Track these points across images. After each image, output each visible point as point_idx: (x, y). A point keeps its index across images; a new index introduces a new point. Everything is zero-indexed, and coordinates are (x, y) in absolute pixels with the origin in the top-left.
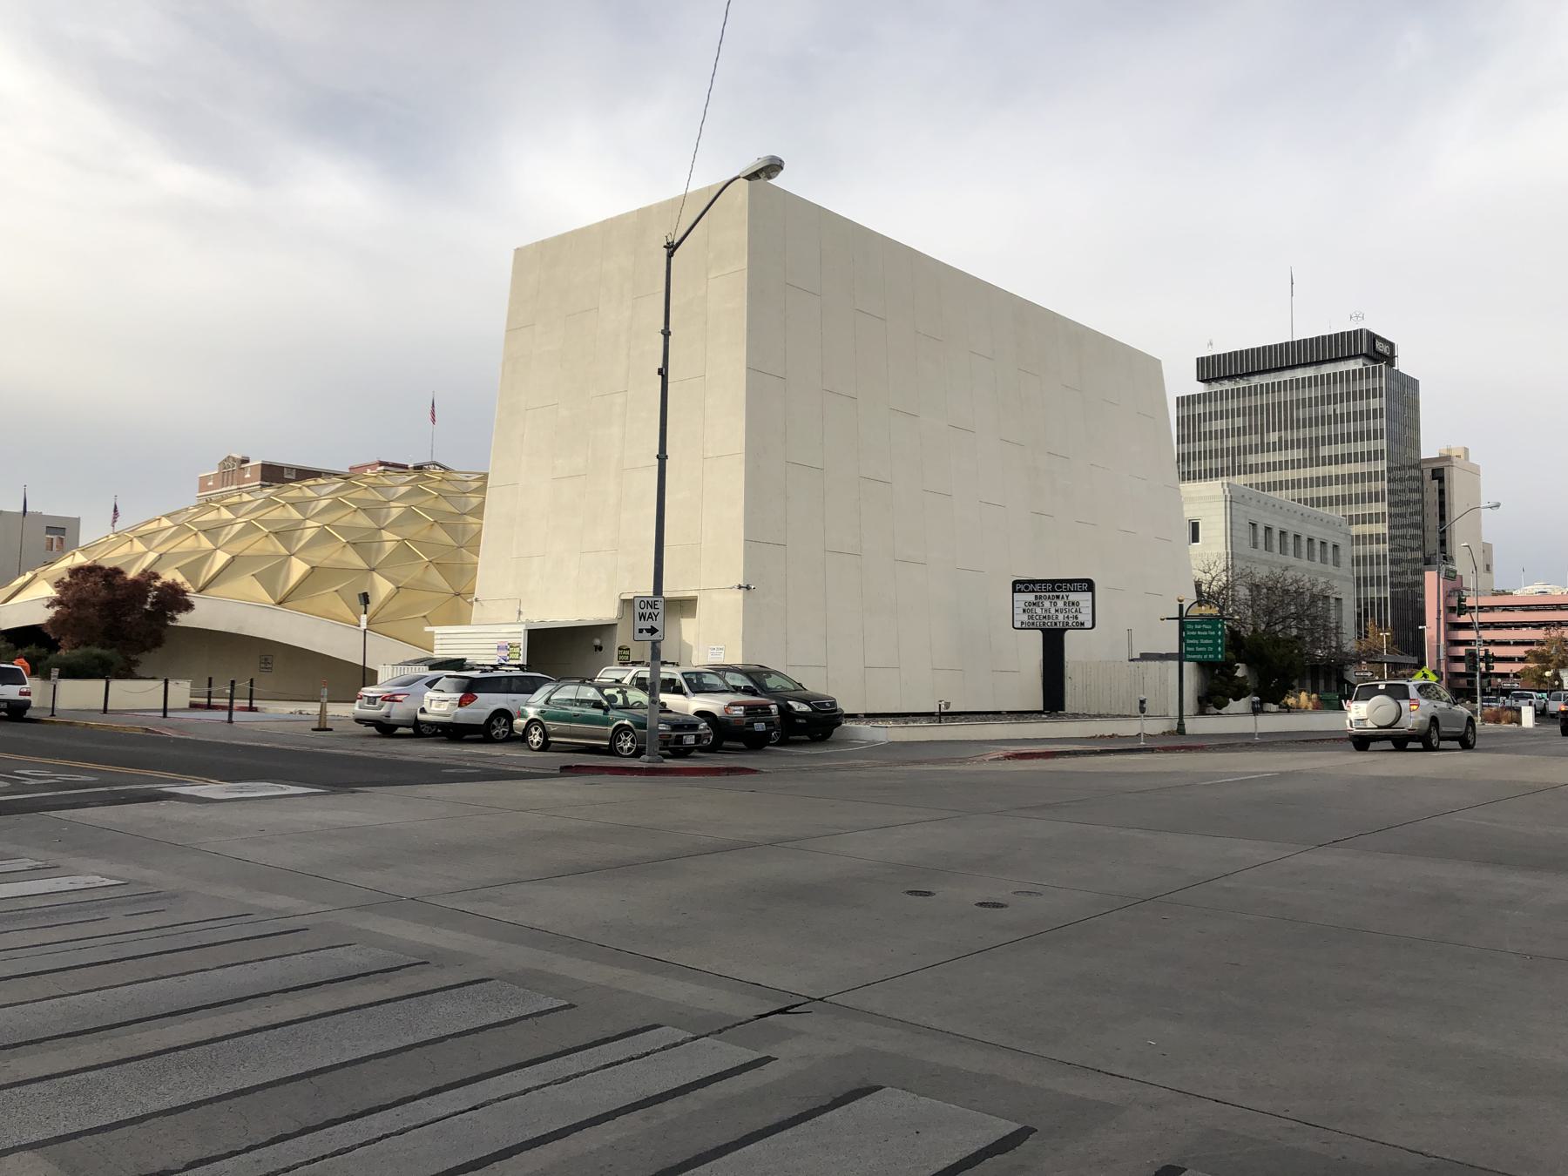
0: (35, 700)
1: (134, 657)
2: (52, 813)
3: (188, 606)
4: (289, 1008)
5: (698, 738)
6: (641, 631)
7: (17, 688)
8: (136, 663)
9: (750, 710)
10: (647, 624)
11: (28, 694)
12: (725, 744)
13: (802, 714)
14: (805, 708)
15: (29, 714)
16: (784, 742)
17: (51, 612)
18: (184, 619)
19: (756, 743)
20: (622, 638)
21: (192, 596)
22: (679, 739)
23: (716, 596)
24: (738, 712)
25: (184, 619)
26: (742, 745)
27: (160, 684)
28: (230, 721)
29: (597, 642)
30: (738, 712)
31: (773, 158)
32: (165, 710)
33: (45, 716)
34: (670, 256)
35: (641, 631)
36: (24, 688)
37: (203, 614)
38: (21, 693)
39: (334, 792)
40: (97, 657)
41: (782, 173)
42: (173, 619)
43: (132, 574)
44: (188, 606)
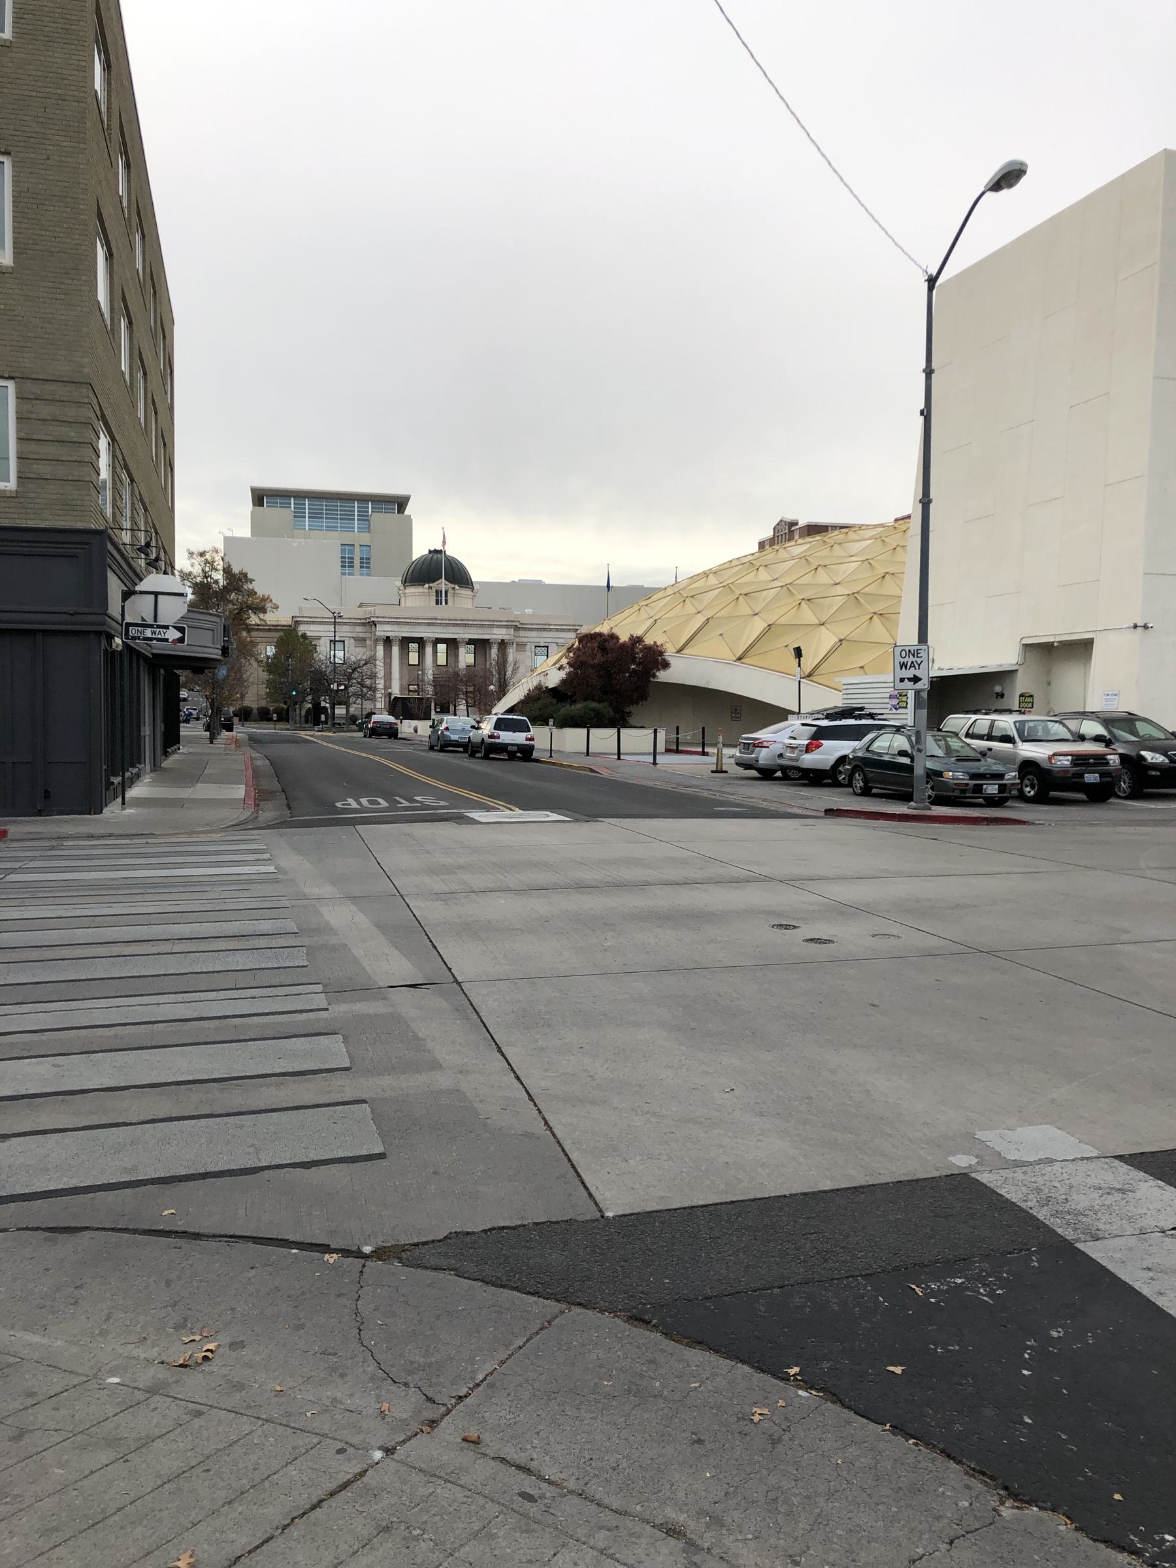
0: (537, 744)
1: (627, 710)
2: (383, 826)
3: (666, 665)
4: (222, 944)
5: (1002, 788)
6: (902, 680)
7: (524, 735)
8: (630, 714)
9: (1080, 760)
10: (910, 673)
11: (532, 739)
12: (1052, 793)
13: (1154, 767)
14: (1160, 759)
15: (535, 755)
16: (1136, 794)
17: (562, 674)
18: (663, 676)
19: (1100, 795)
20: (1021, 684)
21: (670, 654)
22: (978, 789)
23: (1113, 637)
24: (1066, 761)
25: (663, 676)
26: (1082, 796)
27: (649, 732)
28: (655, 763)
29: (998, 689)
30: (1066, 761)
31: (1022, 164)
32: (619, 754)
33: (545, 757)
34: (931, 289)
35: (902, 680)
36: (529, 735)
37: (679, 671)
38: (527, 739)
39: (577, 820)
40: (594, 710)
41: (1024, 180)
42: (654, 676)
43: (624, 638)
44: (666, 665)
